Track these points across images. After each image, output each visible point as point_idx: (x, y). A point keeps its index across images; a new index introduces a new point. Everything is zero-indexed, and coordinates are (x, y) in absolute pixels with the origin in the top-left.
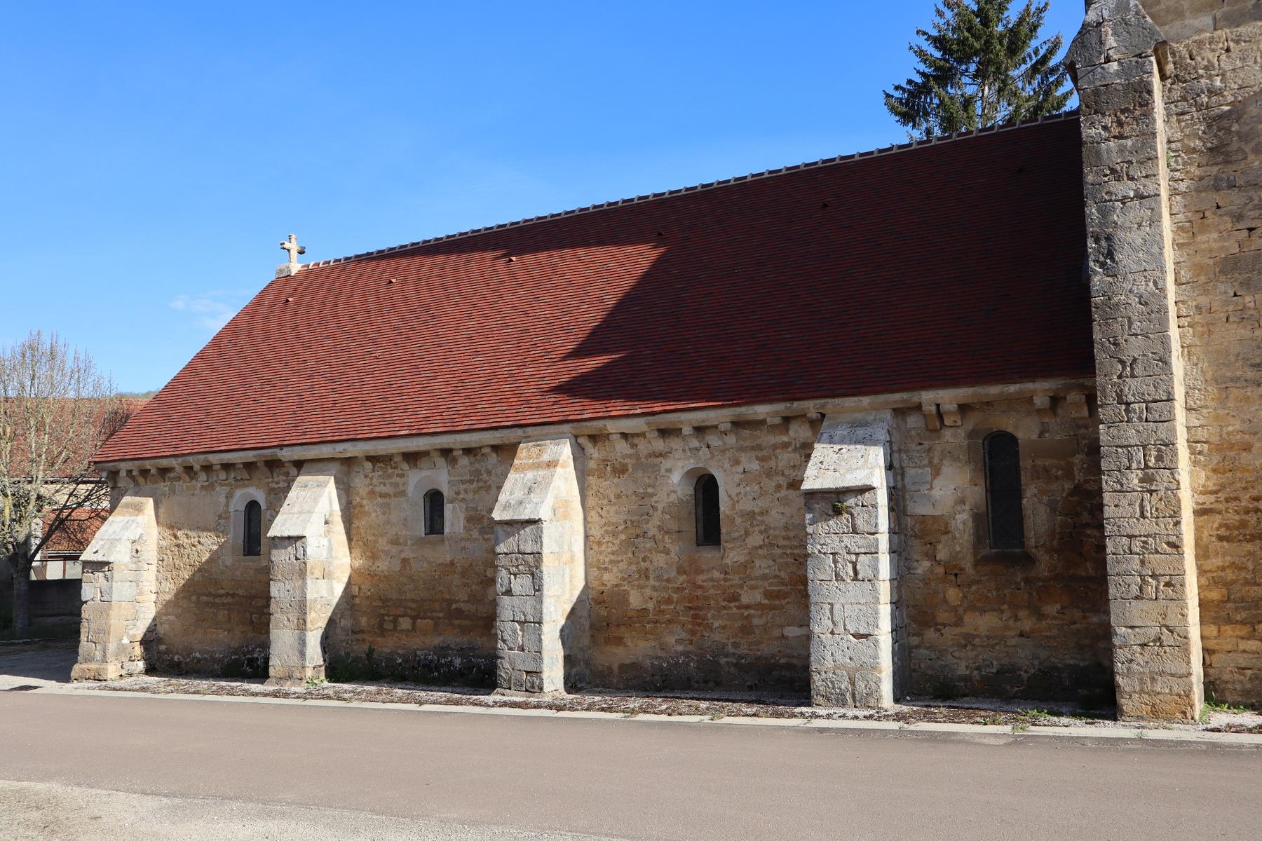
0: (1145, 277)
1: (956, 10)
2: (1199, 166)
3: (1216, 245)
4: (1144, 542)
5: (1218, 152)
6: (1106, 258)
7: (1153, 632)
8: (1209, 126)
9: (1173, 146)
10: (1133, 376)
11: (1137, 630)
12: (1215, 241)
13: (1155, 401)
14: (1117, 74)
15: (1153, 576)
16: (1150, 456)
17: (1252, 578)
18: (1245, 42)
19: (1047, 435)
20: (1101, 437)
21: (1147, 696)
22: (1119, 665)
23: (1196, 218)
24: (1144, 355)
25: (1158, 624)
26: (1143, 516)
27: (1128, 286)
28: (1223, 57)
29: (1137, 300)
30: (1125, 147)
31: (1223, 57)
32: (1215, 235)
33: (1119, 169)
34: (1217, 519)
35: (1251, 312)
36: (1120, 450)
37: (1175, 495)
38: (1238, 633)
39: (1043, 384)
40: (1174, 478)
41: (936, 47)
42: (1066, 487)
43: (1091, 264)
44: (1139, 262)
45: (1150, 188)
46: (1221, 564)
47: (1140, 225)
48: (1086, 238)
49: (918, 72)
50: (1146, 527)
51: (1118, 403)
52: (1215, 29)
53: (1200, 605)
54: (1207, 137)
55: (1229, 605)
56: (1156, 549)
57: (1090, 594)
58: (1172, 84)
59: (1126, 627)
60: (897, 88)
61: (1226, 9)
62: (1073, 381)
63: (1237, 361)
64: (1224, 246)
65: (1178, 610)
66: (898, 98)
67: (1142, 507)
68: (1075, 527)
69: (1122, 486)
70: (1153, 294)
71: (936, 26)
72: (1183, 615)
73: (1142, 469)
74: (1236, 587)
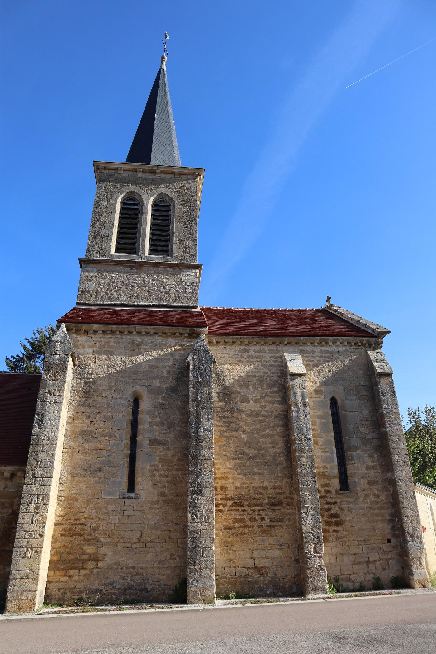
0: (52, 431)
1: (41, 335)
2: (80, 397)
3: (80, 425)
4: (31, 534)
5: (86, 394)
6: (40, 422)
7: (26, 572)
8: (86, 385)
9: (73, 388)
10: (40, 467)
11: (20, 571)
12: (80, 423)
13: (46, 478)
14: (58, 359)
15: (31, 548)
16: (40, 499)
17: (70, 551)
18: (101, 360)
19: (6, 489)
20: (24, 490)
21: (18, 601)
22: (10, 587)
23: (75, 414)
24: (45, 460)
25: (29, 569)
26: (32, 523)
27: (45, 433)
28: (94, 363)
29: (47, 439)
30: (55, 384)
31: (94, 363)
32: (80, 422)
33: (51, 391)
34: (62, 527)
35: (86, 450)
36: (29, 496)
37: (45, 515)
38: (61, 574)
39: (9, 467)
40: (46, 508)
41: (31, 346)
42: (9, 511)
43: (34, 423)
44: (51, 425)
45: (60, 400)
46: (60, 545)
47: (54, 412)
48: (35, 413)
49: (22, 353)
50: (33, 527)
51: (33, 477)
52: (93, 354)
53: (49, 562)
54: (84, 388)
55: (60, 562)
56: (34, 537)
57: (9, 558)
58: (77, 368)
59: (16, 570)
60: (12, 357)
61: (97, 349)
62: (20, 468)
63: (79, 467)
64: (82, 426)
65: (37, 563)
66: (11, 360)
67: (32, 519)
68: (9, 528)
69: (27, 510)
70: (53, 438)
71: (32, 338)
72: (39, 565)
73: (36, 504)
74: (64, 555)
